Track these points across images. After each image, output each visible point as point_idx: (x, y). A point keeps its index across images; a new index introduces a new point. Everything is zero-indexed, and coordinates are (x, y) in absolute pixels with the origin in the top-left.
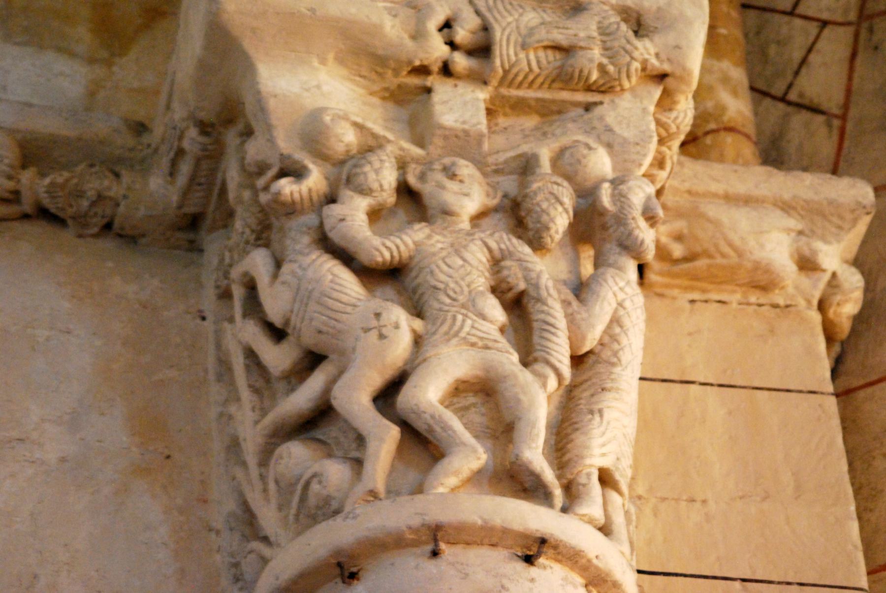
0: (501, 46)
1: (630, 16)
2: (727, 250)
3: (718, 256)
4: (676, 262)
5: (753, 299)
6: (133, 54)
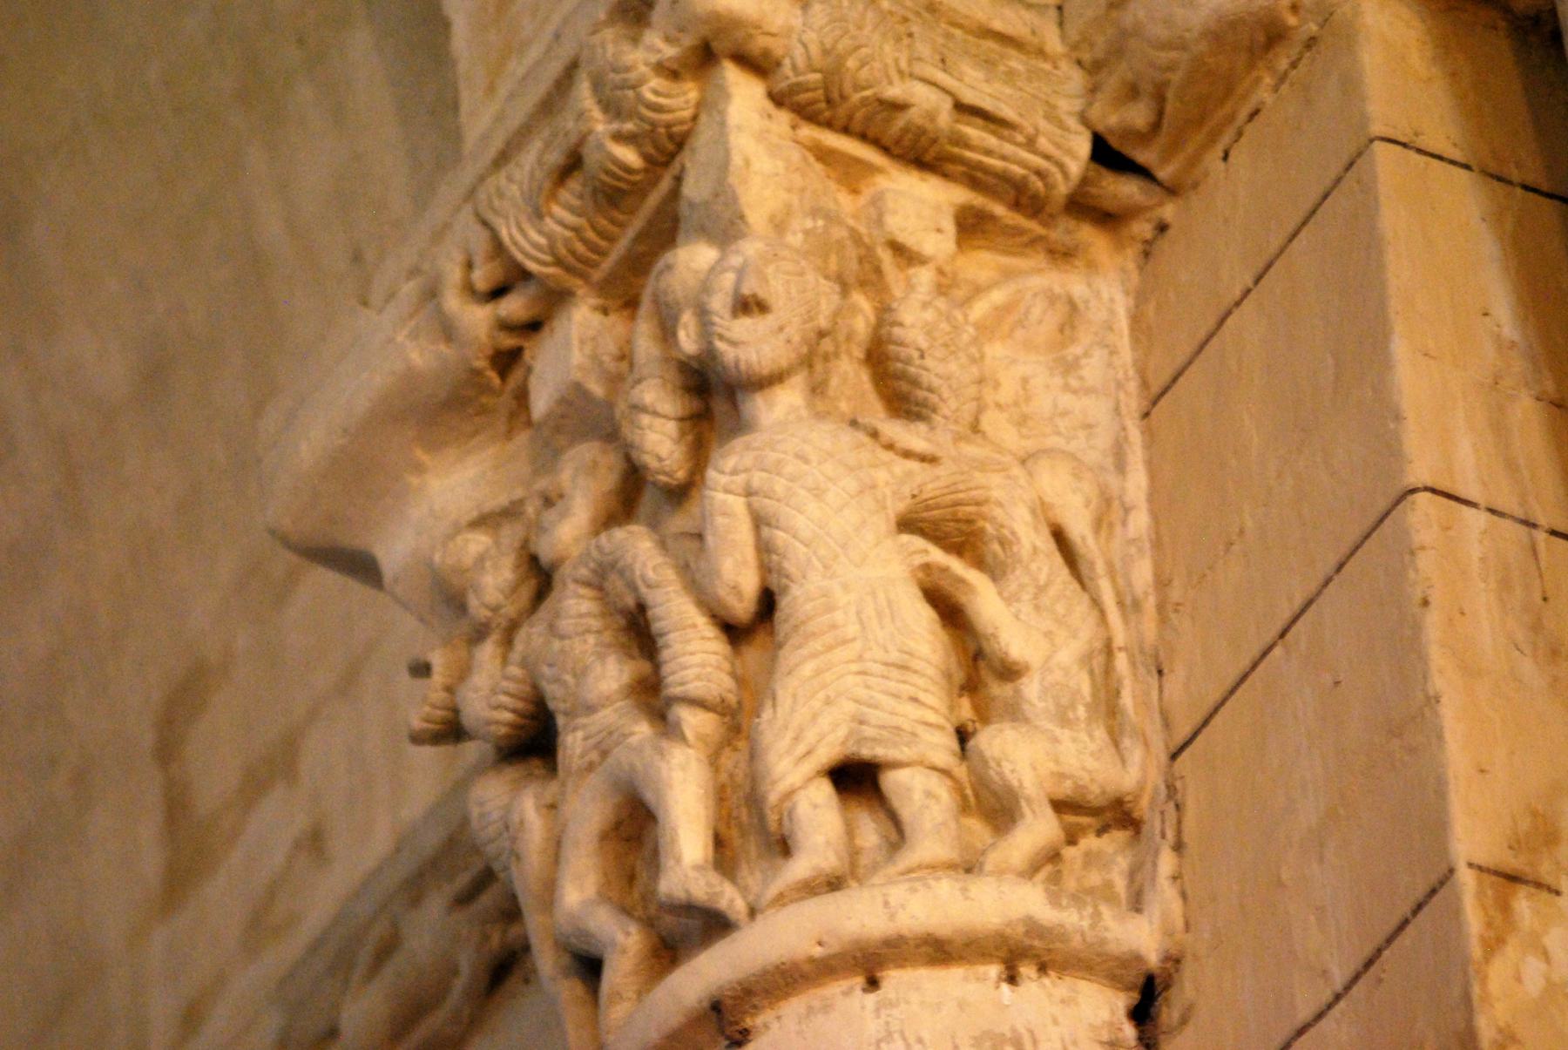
0: (516, 244)
1: (634, 8)
2: (1164, 57)
3: (1170, 75)
4: (1156, 126)
5: (1283, 64)
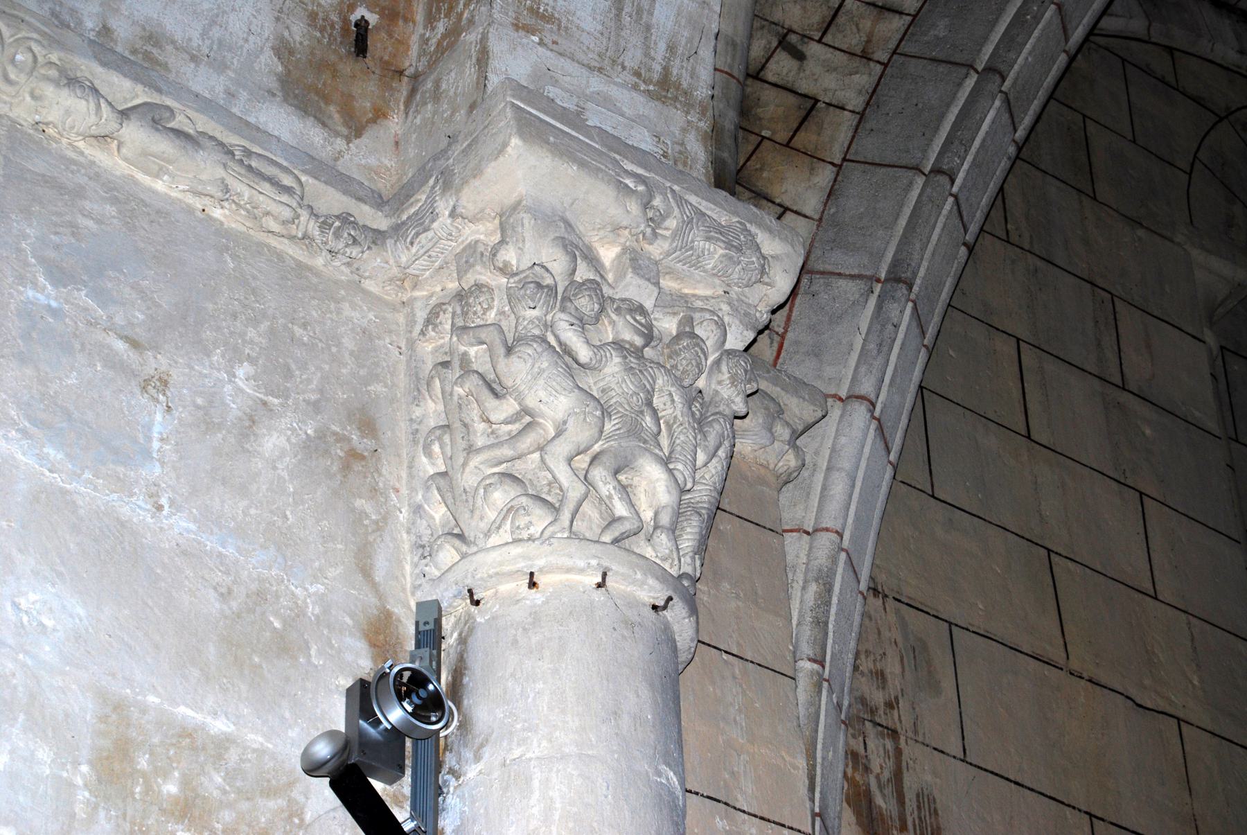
6: (365, 140)
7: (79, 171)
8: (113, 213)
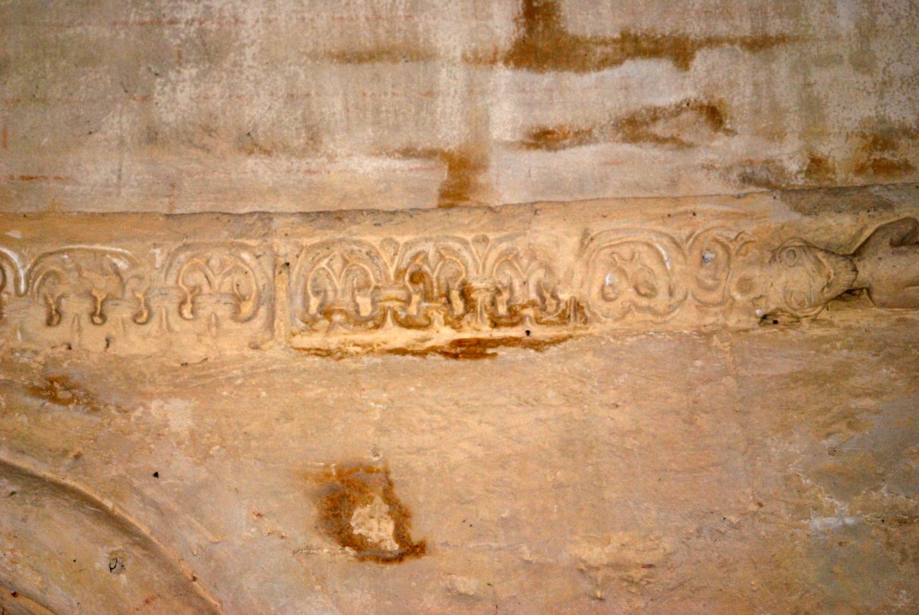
7: (834, 348)
8: (893, 375)
